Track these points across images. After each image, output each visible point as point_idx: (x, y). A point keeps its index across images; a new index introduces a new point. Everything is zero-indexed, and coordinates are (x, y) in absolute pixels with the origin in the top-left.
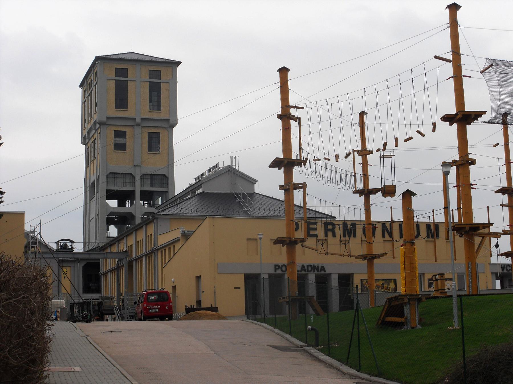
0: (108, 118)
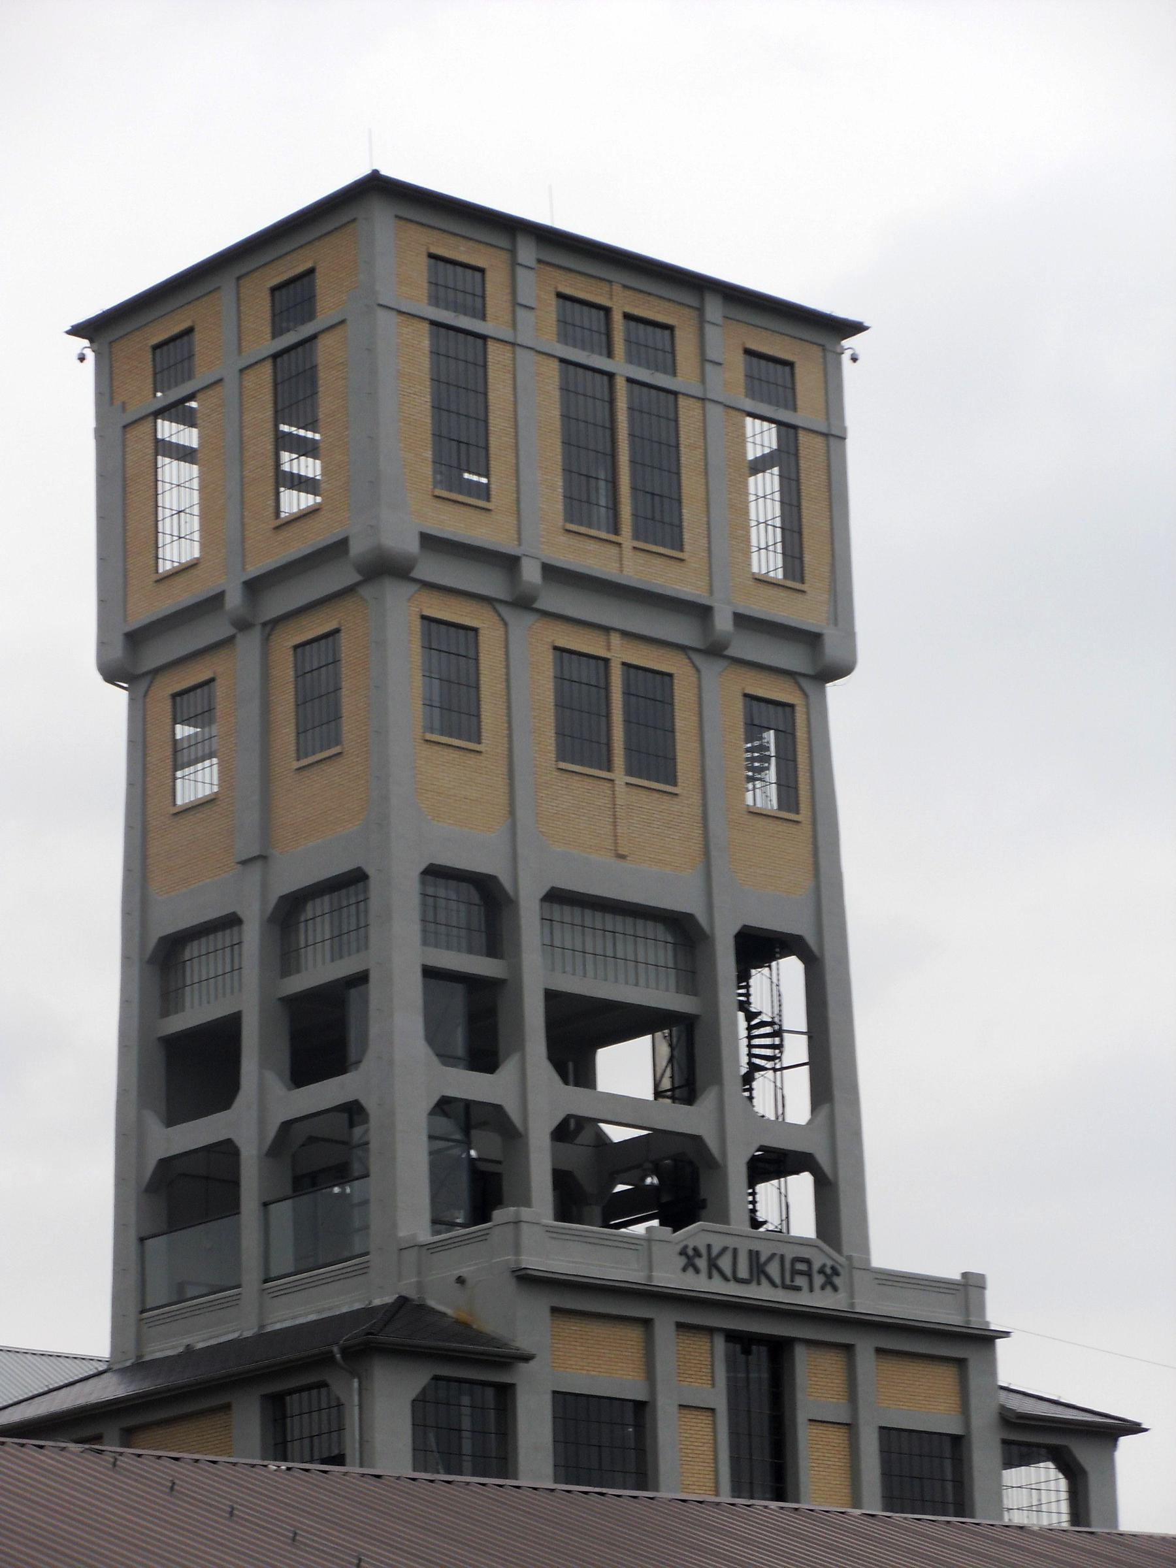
0: (429, 541)
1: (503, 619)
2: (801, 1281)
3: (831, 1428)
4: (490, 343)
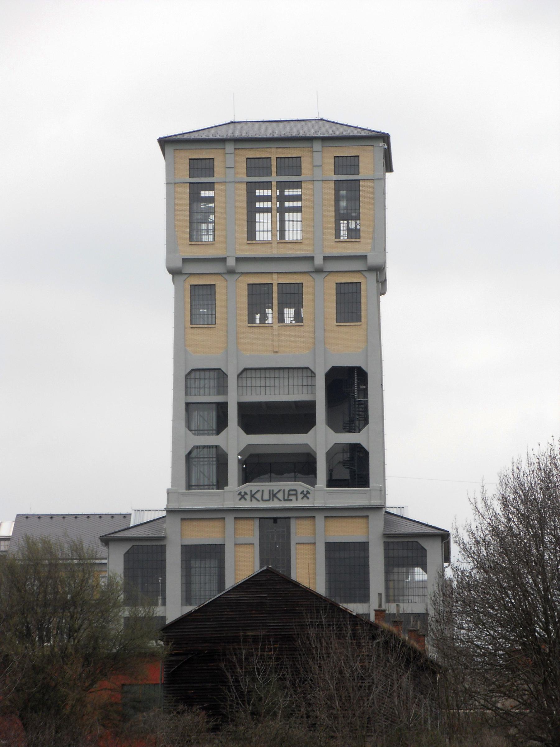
0: (185, 260)
1: (225, 279)
2: (293, 498)
3: (307, 545)
4: (215, 184)
